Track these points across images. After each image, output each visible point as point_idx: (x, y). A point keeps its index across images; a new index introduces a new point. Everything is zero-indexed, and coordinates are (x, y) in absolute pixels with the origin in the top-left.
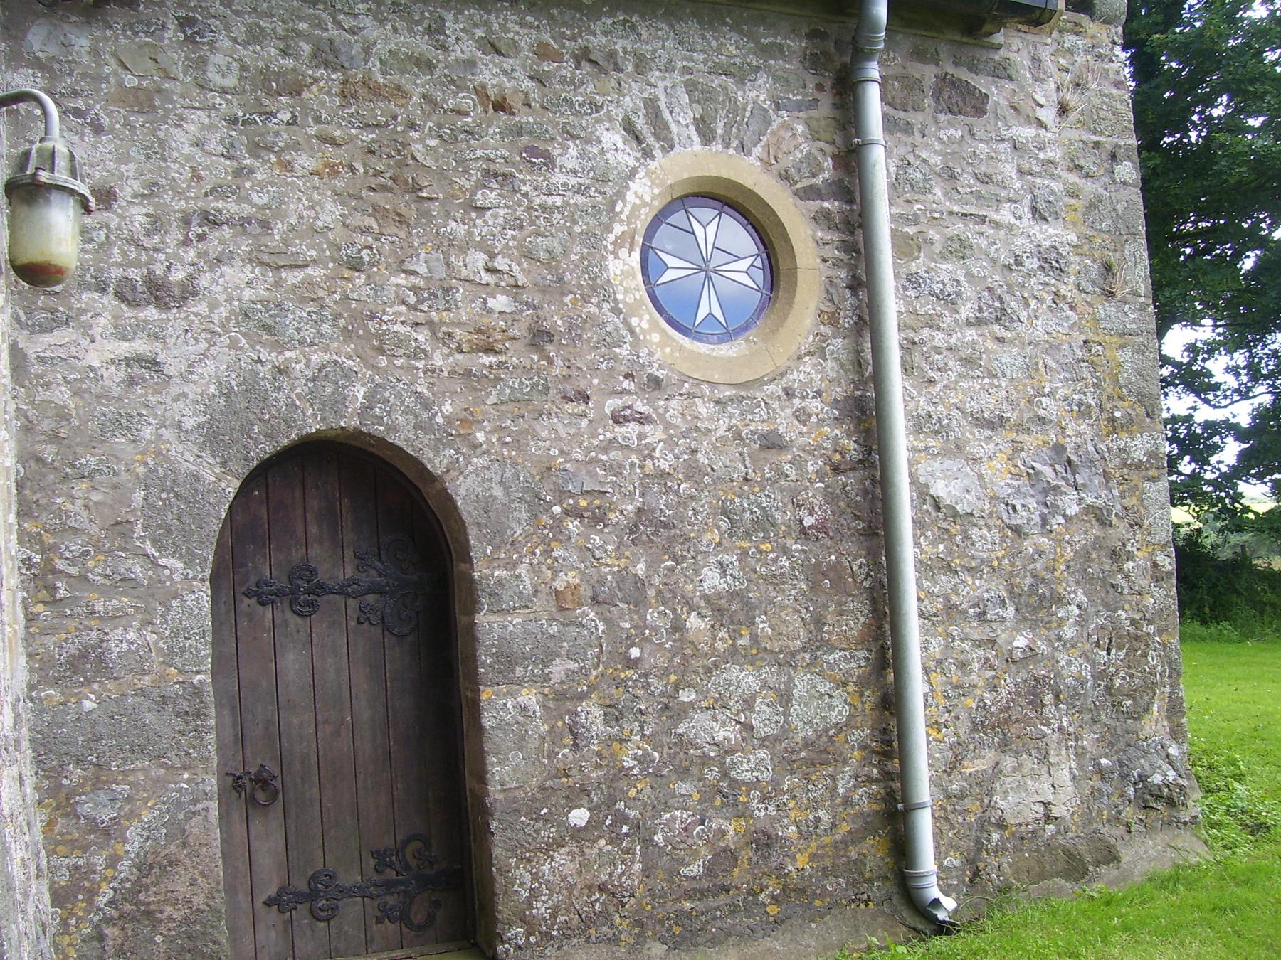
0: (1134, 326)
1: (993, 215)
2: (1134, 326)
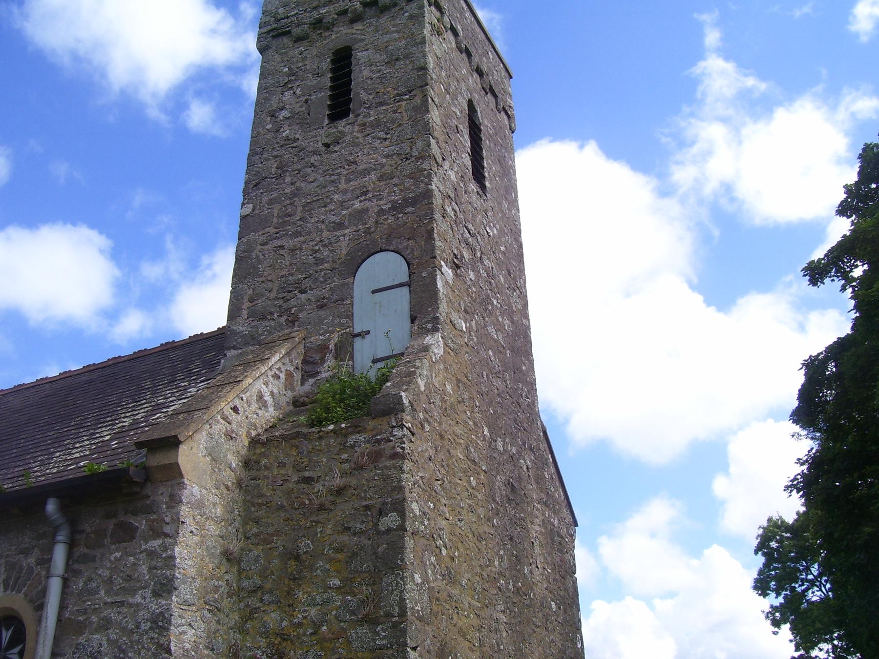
0: (384, 642)
1: (131, 600)
2: (384, 642)
